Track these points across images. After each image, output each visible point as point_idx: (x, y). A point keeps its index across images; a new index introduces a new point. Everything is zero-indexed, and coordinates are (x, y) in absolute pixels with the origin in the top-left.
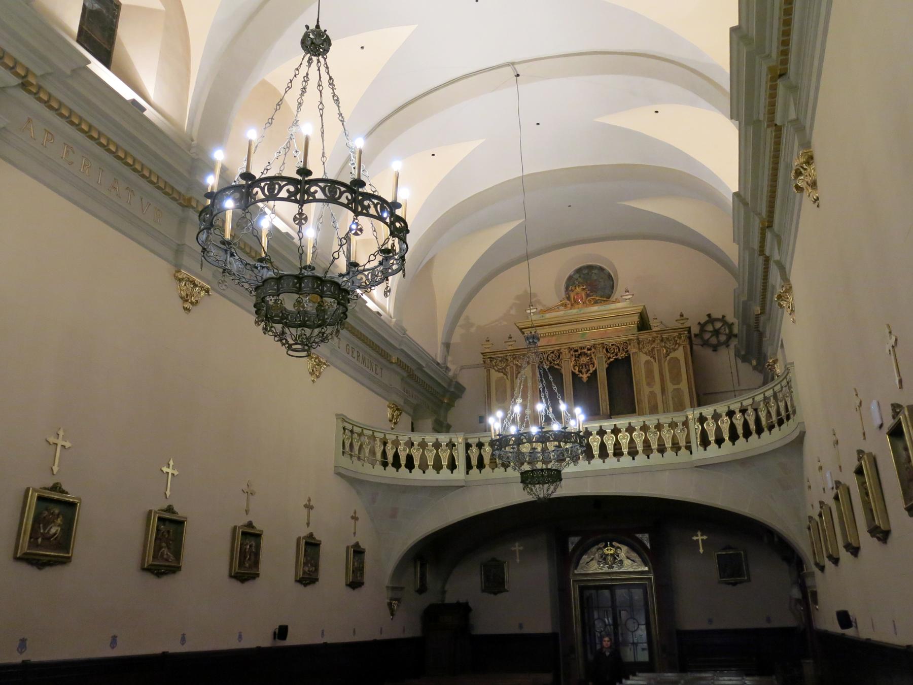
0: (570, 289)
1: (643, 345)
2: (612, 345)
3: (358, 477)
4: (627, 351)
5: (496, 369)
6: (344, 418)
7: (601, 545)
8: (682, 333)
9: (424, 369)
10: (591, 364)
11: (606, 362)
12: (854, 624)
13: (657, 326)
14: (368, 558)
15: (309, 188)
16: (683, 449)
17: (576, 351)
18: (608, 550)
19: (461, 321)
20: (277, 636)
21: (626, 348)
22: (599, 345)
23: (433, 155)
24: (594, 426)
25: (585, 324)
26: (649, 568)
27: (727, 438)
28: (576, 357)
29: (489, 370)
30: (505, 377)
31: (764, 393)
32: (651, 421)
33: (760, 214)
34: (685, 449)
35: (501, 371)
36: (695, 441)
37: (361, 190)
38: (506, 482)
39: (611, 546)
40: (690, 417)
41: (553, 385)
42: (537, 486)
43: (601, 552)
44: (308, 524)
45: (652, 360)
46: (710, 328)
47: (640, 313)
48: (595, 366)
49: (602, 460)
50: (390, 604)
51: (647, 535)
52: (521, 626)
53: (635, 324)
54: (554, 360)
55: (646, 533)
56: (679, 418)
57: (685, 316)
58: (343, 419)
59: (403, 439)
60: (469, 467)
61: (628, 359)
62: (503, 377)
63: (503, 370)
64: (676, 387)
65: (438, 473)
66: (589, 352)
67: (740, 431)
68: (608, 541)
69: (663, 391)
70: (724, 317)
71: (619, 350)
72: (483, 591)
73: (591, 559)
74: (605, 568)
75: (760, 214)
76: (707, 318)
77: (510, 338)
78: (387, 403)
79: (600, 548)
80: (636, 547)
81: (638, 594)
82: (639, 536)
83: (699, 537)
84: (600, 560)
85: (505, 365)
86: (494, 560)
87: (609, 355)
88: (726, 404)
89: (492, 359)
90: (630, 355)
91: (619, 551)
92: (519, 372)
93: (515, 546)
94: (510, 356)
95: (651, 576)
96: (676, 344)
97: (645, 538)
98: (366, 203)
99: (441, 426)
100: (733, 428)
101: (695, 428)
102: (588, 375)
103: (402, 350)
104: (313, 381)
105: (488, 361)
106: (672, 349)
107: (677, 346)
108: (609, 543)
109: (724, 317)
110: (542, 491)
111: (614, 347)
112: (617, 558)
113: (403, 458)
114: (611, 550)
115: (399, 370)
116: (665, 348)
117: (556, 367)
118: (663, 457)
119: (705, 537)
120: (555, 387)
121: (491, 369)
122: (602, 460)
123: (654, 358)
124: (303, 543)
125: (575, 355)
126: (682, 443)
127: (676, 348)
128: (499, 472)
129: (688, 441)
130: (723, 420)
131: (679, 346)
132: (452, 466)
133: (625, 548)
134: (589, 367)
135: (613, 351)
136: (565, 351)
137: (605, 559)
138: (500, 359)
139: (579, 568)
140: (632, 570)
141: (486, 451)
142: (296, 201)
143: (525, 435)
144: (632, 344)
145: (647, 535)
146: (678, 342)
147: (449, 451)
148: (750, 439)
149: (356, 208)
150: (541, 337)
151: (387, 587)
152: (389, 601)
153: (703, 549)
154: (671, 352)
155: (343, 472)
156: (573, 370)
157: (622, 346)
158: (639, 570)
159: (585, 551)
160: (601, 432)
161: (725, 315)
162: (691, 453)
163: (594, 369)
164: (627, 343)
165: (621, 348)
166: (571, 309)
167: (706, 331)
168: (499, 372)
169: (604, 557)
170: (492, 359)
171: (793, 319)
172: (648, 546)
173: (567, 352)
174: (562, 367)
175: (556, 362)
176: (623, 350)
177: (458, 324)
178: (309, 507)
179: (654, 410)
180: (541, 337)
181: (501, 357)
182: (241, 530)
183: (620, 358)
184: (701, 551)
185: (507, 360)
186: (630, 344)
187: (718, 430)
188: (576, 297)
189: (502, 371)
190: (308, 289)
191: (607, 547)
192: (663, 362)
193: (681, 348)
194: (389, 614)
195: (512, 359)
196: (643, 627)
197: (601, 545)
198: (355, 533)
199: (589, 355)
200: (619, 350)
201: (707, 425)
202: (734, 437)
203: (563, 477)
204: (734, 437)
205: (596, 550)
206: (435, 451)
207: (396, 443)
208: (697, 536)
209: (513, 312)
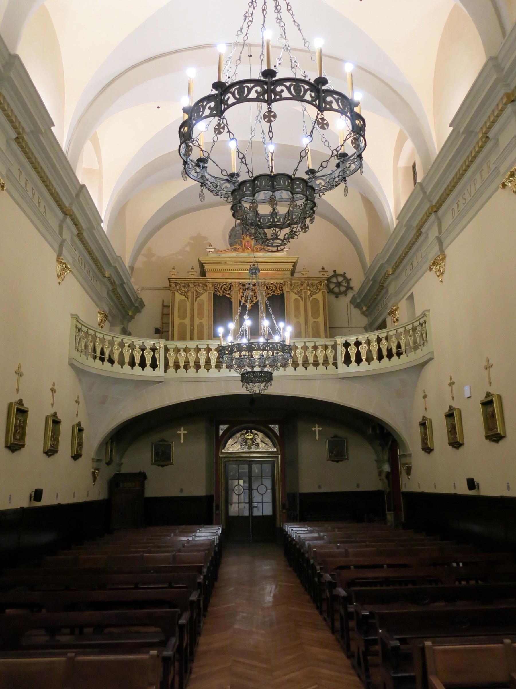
0: (242, 237)
1: (294, 287)
2: (272, 284)
3: (86, 369)
4: (282, 290)
5: (180, 292)
6: (77, 318)
7: (244, 432)
8: (323, 281)
9: (124, 285)
10: (255, 296)
11: (266, 296)
12: (477, 487)
13: (306, 274)
14: (85, 434)
15: (275, 88)
16: (182, 368)
17: (244, 285)
18: (248, 435)
19: (144, 251)
20: (32, 498)
21: (281, 288)
22: (262, 282)
23: (158, 107)
24: (299, 343)
25: (288, 266)
26: (277, 450)
27: (375, 358)
28: (243, 290)
29: (174, 292)
30: (186, 299)
31: (397, 330)
32: (182, 345)
33: (431, 202)
34: (312, 366)
35: (183, 294)
36: (341, 359)
37: (324, 88)
38: (227, 380)
39: (250, 433)
40: (338, 342)
41: (269, 307)
42: (251, 384)
43: (243, 437)
44: (52, 405)
45: (300, 298)
46: (334, 280)
47: (294, 263)
48: (258, 299)
49: (217, 370)
50: (94, 473)
51: (277, 426)
52: (182, 490)
53: (247, 271)
54: (226, 291)
55: (276, 424)
56: (330, 342)
57: (325, 270)
58: (76, 318)
59: (117, 340)
60: (167, 366)
61: (282, 296)
62: (185, 299)
63: (185, 294)
64: (316, 320)
65: (143, 370)
66: (254, 287)
67: (385, 353)
68: (249, 429)
69: (306, 322)
70: (345, 273)
71: (276, 288)
72: (153, 464)
73: (235, 441)
74: (245, 448)
75: (431, 202)
76: (343, 273)
77: (193, 269)
78: (98, 310)
79: (242, 434)
80: (269, 434)
81: (267, 468)
82: (272, 426)
83: (317, 429)
84: (242, 443)
85: (187, 289)
86: (163, 440)
87: (268, 291)
88: (376, 333)
89: (176, 284)
90: (284, 293)
91: (256, 437)
92: (198, 297)
93: (181, 431)
94: (192, 283)
95: (279, 455)
96: (318, 289)
97: (276, 428)
98: (279, 89)
99: (125, 332)
100: (380, 351)
101: (341, 351)
102: (252, 304)
103: (115, 268)
104: (59, 283)
105: (173, 285)
106: (315, 292)
107: (318, 290)
108: (249, 431)
109: (345, 273)
110: (257, 388)
111: (272, 285)
112: (255, 441)
113: (394, 348)
114: (250, 435)
115: (108, 283)
116: (310, 291)
117: (228, 296)
118: (316, 369)
119: (320, 429)
120: (271, 310)
121: (175, 291)
122: (217, 370)
123: (301, 297)
124: (51, 420)
125: (243, 288)
126: (331, 360)
127: (317, 291)
128: (225, 372)
129: (335, 358)
130: (362, 347)
131: (320, 291)
132: (154, 365)
133: (261, 435)
134: (253, 299)
135: (272, 288)
136: (235, 285)
137: (246, 442)
138: (183, 285)
139: (226, 448)
140: (265, 450)
141: (171, 356)
142: (264, 101)
143: (255, 344)
144: (286, 285)
145: (277, 426)
146: (319, 287)
147: (152, 353)
148: (392, 359)
149: (269, 97)
150: (207, 271)
151: (92, 459)
152: (94, 470)
153: (183, 440)
154: (313, 294)
155: (75, 363)
156: (241, 300)
157: (279, 286)
158: (270, 450)
159: (231, 437)
160: (305, 348)
161: (346, 272)
162: (337, 368)
163: (256, 300)
164: (282, 284)
165: (278, 288)
166: (242, 253)
167: (332, 282)
168: (182, 295)
169: (245, 441)
170: (176, 284)
171: (442, 280)
172: (278, 433)
173: (237, 286)
174: (232, 297)
175: (227, 292)
176: (280, 289)
177: (142, 253)
178: (53, 390)
179: (182, 338)
180: (207, 271)
181: (185, 283)
182: (16, 407)
183: (277, 295)
184: (317, 438)
185: (189, 286)
186: (284, 285)
187: (369, 352)
188: (246, 244)
189: (185, 294)
190: (249, 192)
191: (248, 433)
192: (307, 301)
193: (321, 293)
194: (92, 480)
195: (193, 286)
196: (270, 491)
197: (243, 432)
198: (77, 415)
199: (253, 289)
200: (276, 288)
201: (350, 349)
202: (380, 357)
203: (273, 378)
204: (380, 357)
205: (239, 436)
206: (141, 352)
207: (111, 343)
208: (315, 427)
209: (188, 249)
